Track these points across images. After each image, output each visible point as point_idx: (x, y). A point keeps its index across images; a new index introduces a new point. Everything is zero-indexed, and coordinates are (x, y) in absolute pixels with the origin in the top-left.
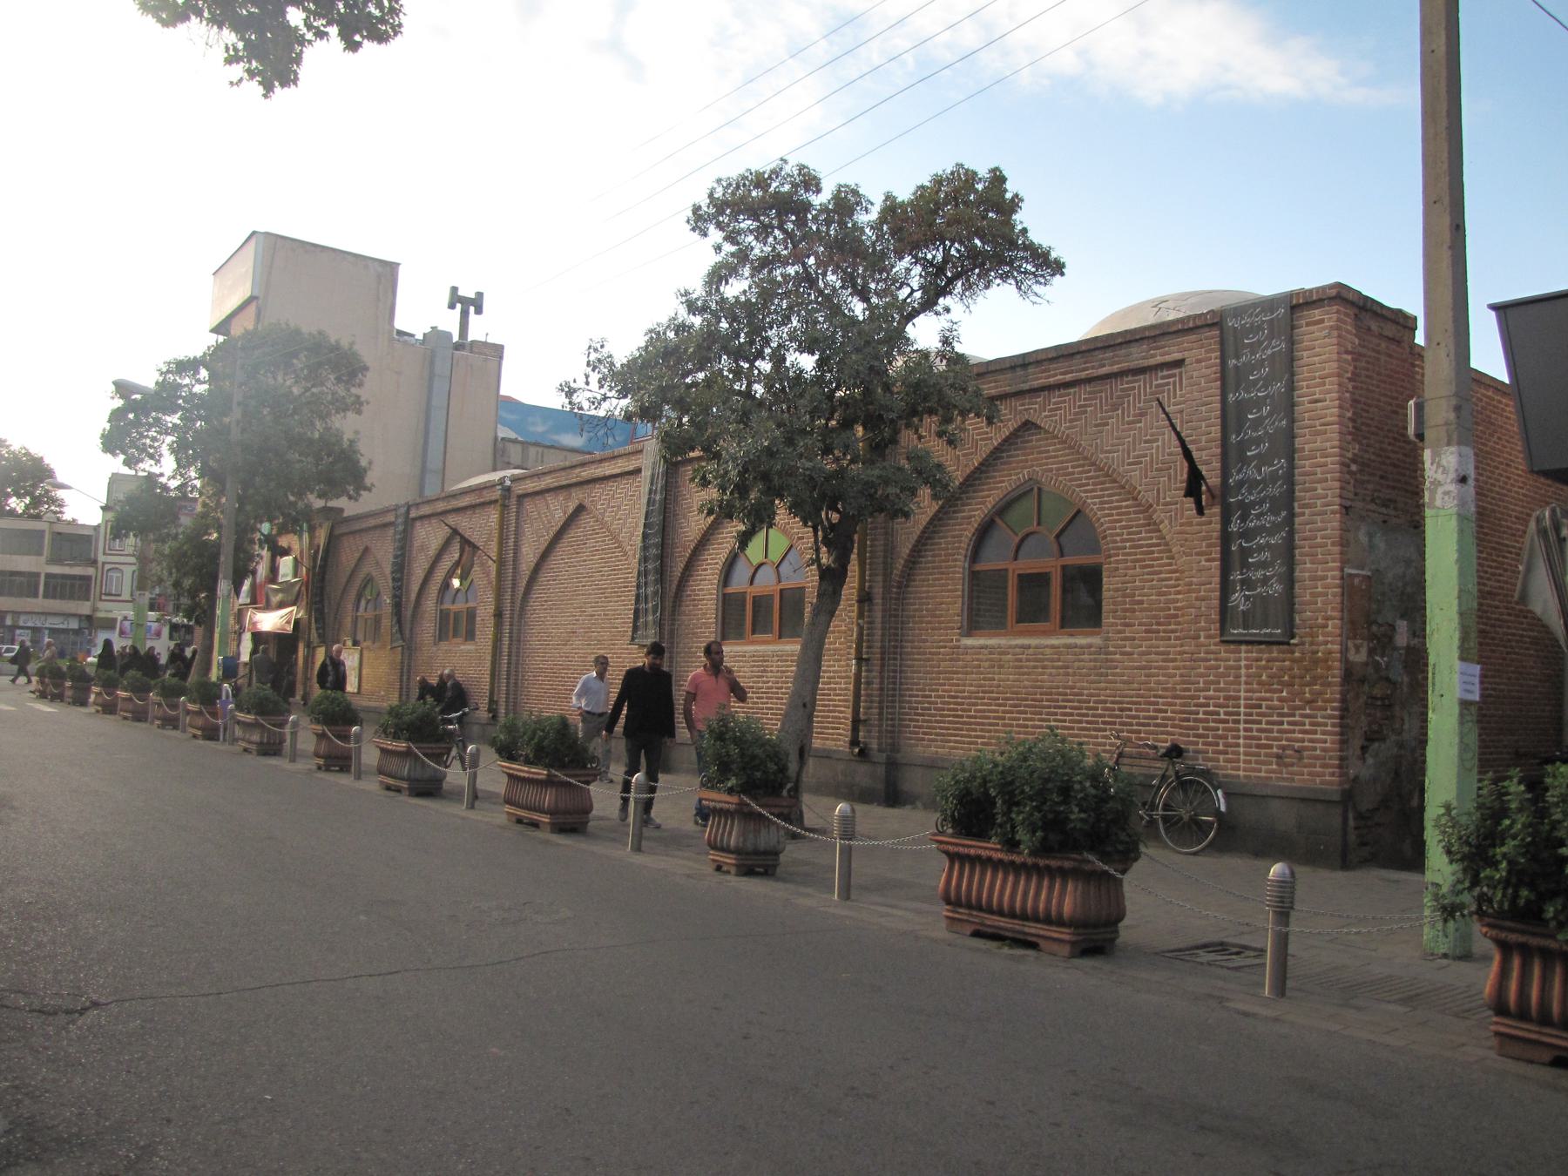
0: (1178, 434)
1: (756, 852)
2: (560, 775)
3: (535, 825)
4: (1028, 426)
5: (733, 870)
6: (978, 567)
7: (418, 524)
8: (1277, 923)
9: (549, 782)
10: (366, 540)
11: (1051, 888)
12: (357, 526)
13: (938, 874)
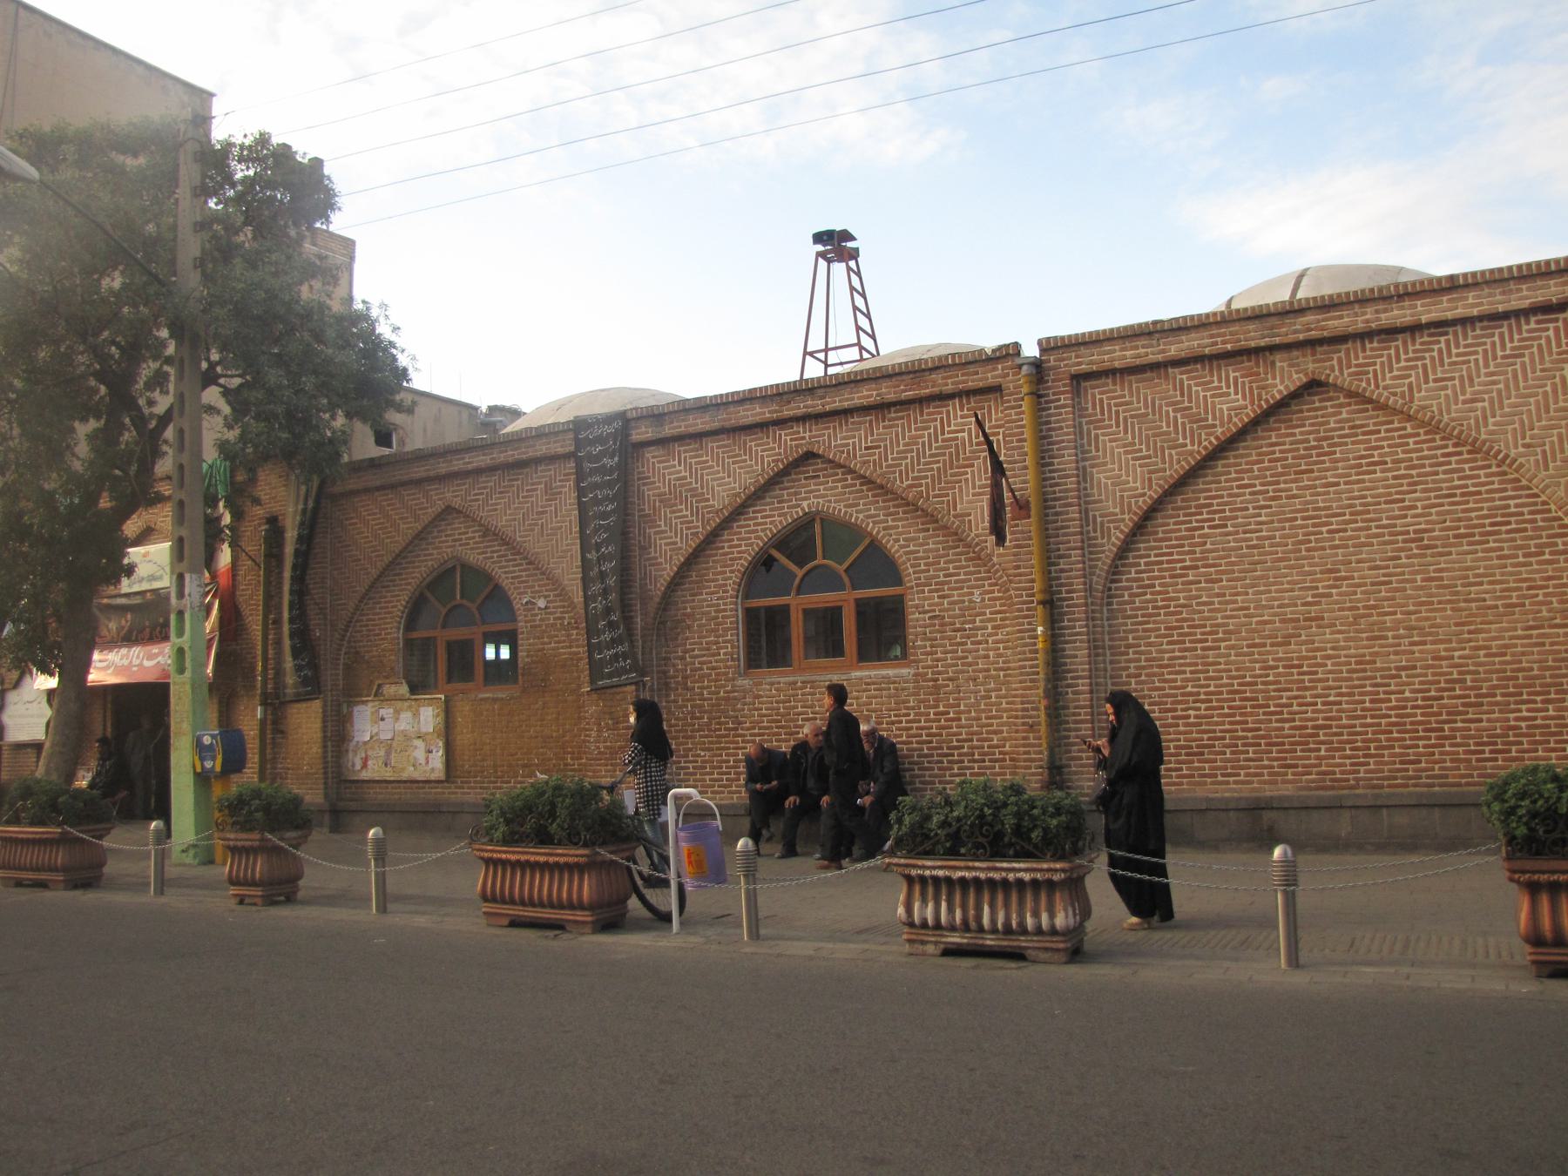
0: (993, 455)
2: (605, 854)
4: (449, 510)
5: (259, 901)
6: (415, 635)
7: (651, 454)
8: (747, 883)
9: (64, 840)
10: (452, 495)
11: (495, 873)
13: (478, 879)
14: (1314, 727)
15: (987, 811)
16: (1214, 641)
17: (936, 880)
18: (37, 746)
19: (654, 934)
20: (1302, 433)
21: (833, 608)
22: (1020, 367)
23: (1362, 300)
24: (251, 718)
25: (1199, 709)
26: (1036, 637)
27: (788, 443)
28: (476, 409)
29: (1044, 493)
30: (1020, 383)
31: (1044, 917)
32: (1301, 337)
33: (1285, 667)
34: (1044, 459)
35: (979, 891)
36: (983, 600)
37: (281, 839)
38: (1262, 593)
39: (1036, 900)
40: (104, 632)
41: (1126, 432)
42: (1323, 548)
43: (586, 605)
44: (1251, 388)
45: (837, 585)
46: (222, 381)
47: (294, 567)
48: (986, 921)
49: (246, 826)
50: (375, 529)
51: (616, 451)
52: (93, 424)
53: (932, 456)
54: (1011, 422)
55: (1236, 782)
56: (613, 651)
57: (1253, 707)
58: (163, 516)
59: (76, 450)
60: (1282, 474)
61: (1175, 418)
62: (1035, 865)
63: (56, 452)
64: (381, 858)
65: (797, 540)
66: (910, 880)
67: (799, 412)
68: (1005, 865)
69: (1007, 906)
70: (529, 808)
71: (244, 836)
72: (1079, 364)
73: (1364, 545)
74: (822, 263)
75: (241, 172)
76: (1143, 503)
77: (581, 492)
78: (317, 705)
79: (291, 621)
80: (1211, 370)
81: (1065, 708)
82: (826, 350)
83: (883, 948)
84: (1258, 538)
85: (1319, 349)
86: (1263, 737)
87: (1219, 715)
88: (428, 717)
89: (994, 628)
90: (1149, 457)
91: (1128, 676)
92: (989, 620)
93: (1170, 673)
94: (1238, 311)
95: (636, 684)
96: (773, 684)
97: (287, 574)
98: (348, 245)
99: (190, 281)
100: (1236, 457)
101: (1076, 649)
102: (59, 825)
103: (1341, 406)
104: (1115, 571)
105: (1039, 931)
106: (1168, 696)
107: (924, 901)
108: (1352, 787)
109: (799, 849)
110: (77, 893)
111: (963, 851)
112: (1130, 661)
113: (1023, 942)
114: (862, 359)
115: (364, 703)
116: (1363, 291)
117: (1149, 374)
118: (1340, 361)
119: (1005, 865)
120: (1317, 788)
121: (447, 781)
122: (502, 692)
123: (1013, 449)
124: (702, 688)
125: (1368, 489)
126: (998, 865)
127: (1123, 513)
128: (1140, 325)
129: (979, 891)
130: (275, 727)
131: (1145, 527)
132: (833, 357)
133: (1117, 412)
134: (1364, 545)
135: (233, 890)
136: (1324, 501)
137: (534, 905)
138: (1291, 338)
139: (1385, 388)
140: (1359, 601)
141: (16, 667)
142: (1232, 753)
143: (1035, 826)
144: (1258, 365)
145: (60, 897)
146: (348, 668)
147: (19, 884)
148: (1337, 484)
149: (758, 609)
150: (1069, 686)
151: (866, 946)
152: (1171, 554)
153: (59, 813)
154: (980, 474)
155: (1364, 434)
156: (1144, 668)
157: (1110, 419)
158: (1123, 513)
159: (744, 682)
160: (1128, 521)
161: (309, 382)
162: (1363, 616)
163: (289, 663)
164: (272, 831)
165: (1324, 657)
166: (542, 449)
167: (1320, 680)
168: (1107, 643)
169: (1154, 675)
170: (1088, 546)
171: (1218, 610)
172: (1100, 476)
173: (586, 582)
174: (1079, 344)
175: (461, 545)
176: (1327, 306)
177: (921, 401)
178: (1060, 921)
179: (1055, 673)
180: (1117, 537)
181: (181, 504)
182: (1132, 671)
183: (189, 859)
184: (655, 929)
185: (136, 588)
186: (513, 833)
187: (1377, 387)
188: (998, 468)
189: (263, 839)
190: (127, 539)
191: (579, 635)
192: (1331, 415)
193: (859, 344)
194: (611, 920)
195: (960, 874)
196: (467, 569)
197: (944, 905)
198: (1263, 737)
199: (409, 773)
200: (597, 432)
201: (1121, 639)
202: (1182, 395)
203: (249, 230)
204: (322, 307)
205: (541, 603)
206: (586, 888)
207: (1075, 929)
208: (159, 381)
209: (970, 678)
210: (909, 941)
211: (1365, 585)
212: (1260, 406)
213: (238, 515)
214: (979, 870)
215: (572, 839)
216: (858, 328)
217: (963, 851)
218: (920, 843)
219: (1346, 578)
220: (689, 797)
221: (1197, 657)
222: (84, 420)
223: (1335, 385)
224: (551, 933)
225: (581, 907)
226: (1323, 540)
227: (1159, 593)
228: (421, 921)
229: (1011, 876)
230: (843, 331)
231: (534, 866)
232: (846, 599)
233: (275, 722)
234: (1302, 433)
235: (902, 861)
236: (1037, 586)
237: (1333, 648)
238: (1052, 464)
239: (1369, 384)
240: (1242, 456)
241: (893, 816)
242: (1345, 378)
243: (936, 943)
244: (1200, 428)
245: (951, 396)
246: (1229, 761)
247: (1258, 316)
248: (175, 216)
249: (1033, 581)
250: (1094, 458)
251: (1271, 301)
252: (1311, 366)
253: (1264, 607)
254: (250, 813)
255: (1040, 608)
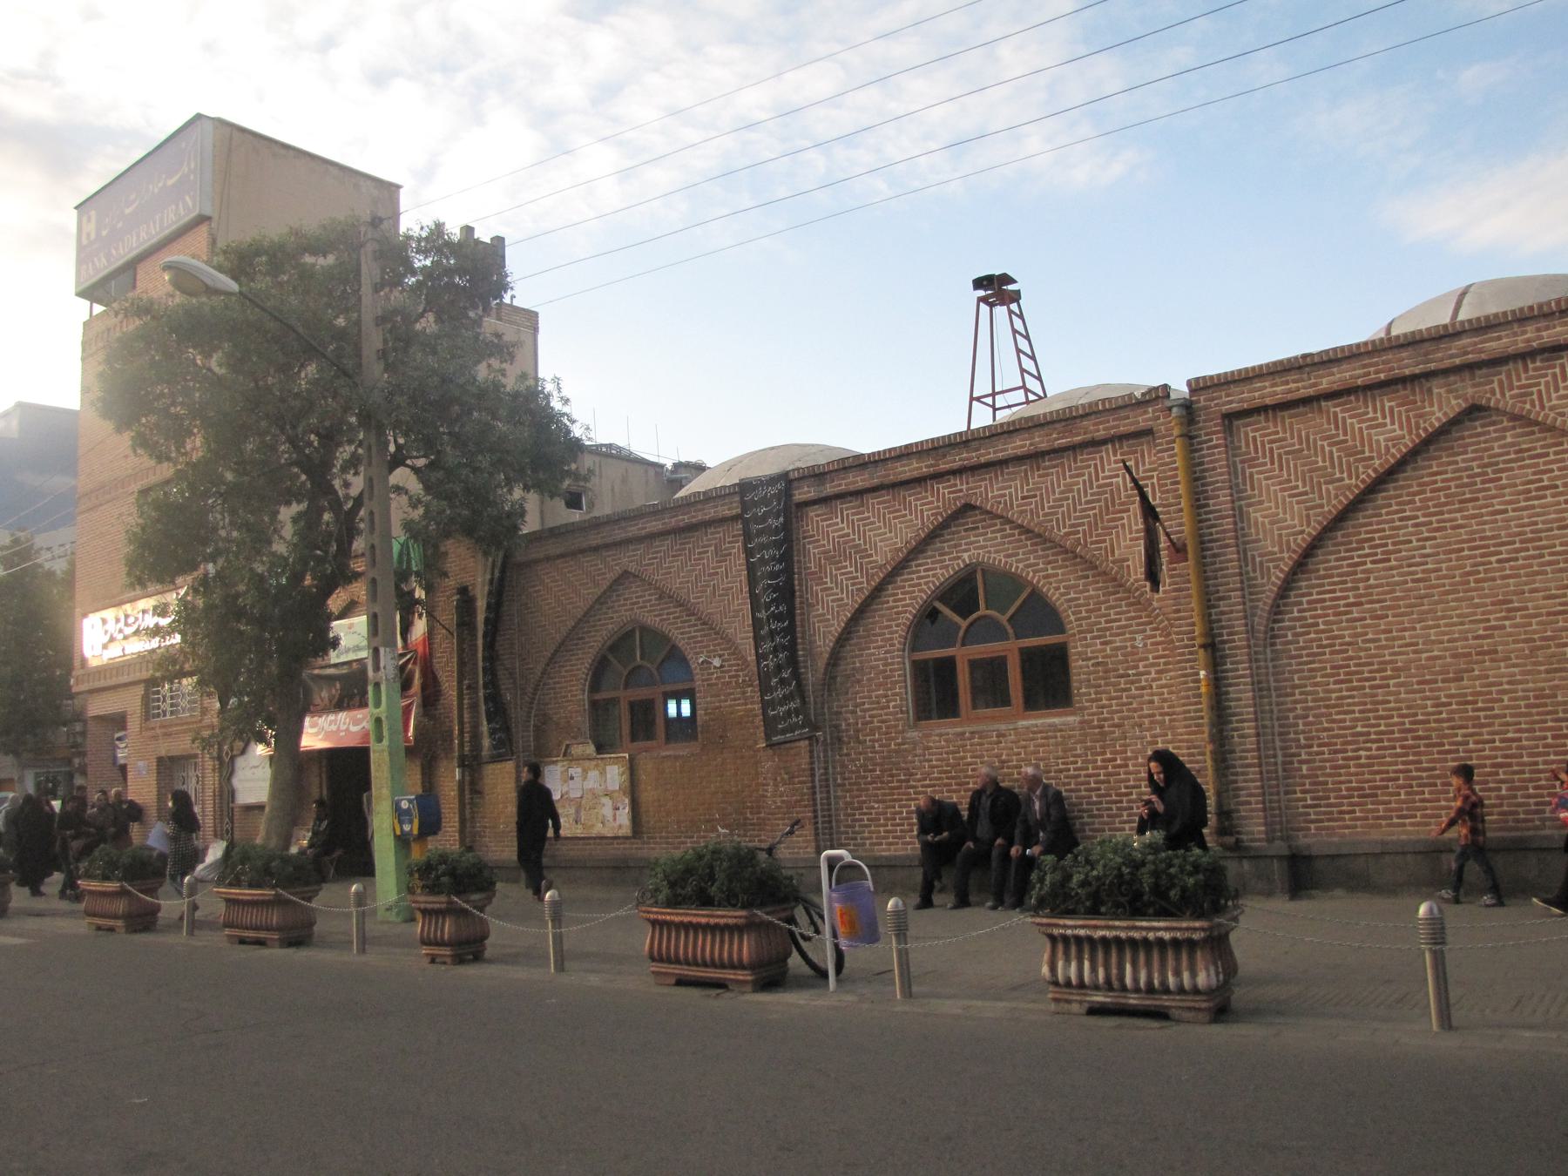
1: (468, 942)
3: (111, 929)
4: (626, 574)
5: (448, 960)
6: (597, 697)
7: (813, 513)
8: (899, 943)
9: (278, 902)
10: (627, 560)
12: (594, 539)
13: (645, 940)
14: (1493, 766)
15: (1126, 870)
16: (1382, 678)
17: (1078, 939)
18: (260, 807)
19: (812, 992)
20: (1464, 461)
21: (993, 660)
22: (1170, 409)
23: (1522, 318)
24: (450, 777)
25: (1370, 749)
26: (1198, 681)
27: (945, 496)
28: (662, 466)
29: (1201, 536)
30: (1169, 426)
31: (1186, 976)
32: (1457, 361)
33: (1458, 703)
34: (1199, 500)
35: (1121, 951)
36: (1145, 645)
37: (467, 902)
38: (1430, 627)
39: (1178, 959)
40: (317, 701)
41: (1281, 470)
42: (1494, 579)
43: (758, 663)
44: (1408, 418)
45: (1003, 636)
46: (409, 462)
47: (485, 636)
48: (1128, 980)
49: (433, 889)
50: (559, 596)
51: (783, 507)
52: (295, 508)
53: (1087, 502)
54: (1161, 467)
55: (1412, 824)
56: (786, 708)
57: (1427, 746)
58: (359, 590)
59: (283, 533)
60: (1446, 504)
61: (1331, 453)
62: (1175, 924)
63: (260, 538)
64: (557, 919)
65: (961, 593)
66: (1053, 938)
67: (955, 465)
68: (1144, 924)
69: (1149, 964)
70: (689, 871)
71: (431, 899)
72: (1231, 402)
73: (1538, 573)
74: (984, 308)
75: (421, 262)
76: (1302, 541)
77: (749, 553)
78: (509, 766)
79: (485, 686)
80: (1366, 402)
81: (1233, 752)
82: (994, 394)
83: (1031, 1006)
84: (1424, 571)
85: (1478, 372)
86: (1438, 777)
87: (1391, 756)
88: (615, 775)
89: (1158, 672)
90: (1306, 493)
91: (1296, 717)
92: (1153, 665)
93: (1339, 713)
94: (1398, 337)
95: (809, 738)
96: (943, 732)
97: (480, 642)
98: (530, 319)
99: (375, 373)
100: (1395, 489)
101: (1240, 692)
102: (273, 887)
103: (1505, 429)
104: (1277, 611)
105: (1181, 990)
106: (1338, 736)
107: (1068, 961)
108: (1537, 828)
109: (972, 898)
110: (291, 951)
111: (1103, 909)
112: (1296, 702)
113: (1165, 1001)
114: (1028, 402)
115: (555, 763)
116: (1521, 309)
117: (1301, 409)
118: (1501, 383)
119: (1144, 924)
120: (1501, 829)
121: (634, 837)
122: (681, 749)
123: (1168, 492)
124: (873, 741)
125: (1538, 515)
126: (1138, 924)
127: (1282, 551)
128: (1289, 360)
129: (1121, 951)
130: (472, 788)
131: (1306, 564)
132: (1000, 401)
133: (1271, 450)
134: (1538, 573)
135: (425, 950)
136: (1492, 529)
137: (697, 965)
138: (1447, 363)
139: (1551, 409)
140: (1535, 632)
141: (241, 739)
142: (1407, 793)
143: (1173, 886)
144: (1414, 394)
145: (277, 953)
146: (537, 729)
147: (242, 941)
148: (1506, 511)
149: (926, 662)
150: (1236, 729)
151: (1014, 1004)
152: (1334, 591)
153: (271, 875)
154: (1134, 520)
155: (1531, 457)
156: (1311, 708)
157: (1264, 456)
158: (1282, 551)
159: (913, 734)
160: (1287, 560)
161: (484, 461)
162: (1542, 648)
163: (485, 727)
164: (458, 894)
165: (1499, 692)
166: (711, 512)
167: (1496, 716)
168: (1273, 684)
169: (1322, 715)
170: (1248, 587)
171: (1386, 647)
172: (1256, 515)
173: (757, 639)
174: (1227, 383)
175: (638, 608)
176: (1484, 327)
177: (1073, 448)
178: (1202, 980)
179: (1219, 716)
180: (1277, 577)
181: (374, 581)
182: (1299, 712)
183: (392, 916)
184: (813, 986)
185: (343, 659)
186: (676, 896)
187: (1542, 407)
188: (1150, 513)
189: (450, 902)
190: (331, 613)
191: (753, 692)
192: (1497, 440)
193: (1024, 387)
194: (772, 978)
195: (1101, 933)
196: (644, 629)
197: (1087, 964)
198: (1438, 777)
199: (598, 829)
200: (761, 492)
201: (1286, 680)
202: (1337, 428)
203: (431, 317)
204: (497, 386)
205: (717, 662)
206: (746, 948)
207: (1219, 988)
208: (353, 463)
209: (1136, 724)
210: (1056, 1000)
211: (1540, 615)
212: (1418, 435)
213: (429, 589)
214: (1102, 929)
215: (730, 901)
216: (1023, 371)
217: (1103, 909)
218: (1060, 902)
219: (1519, 609)
220: (840, 858)
221: (1365, 695)
222: (288, 503)
223: (1497, 409)
224: (713, 992)
225: (741, 966)
226: (1494, 570)
227: (1323, 631)
228: (594, 980)
229: (1151, 936)
230: (1009, 376)
231: (696, 927)
232: (1010, 649)
233: (472, 783)
234: (1464, 461)
235: (1045, 921)
236: (1198, 630)
237: (1509, 683)
238: (1207, 505)
239: (1533, 405)
240: (1402, 487)
241: (1034, 876)
242: (1508, 401)
243: (1081, 1002)
244: (1356, 461)
245: (1104, 442)
246: (1404, 802)
247: (1413, 342)
248: (359, 311)
249: (1193, 624)
250: (1249, 497)
251: (1423, 327)
252: (1470, 391)
253: (1433, 642)
254: (438, 878)
255: (1201, 651)
